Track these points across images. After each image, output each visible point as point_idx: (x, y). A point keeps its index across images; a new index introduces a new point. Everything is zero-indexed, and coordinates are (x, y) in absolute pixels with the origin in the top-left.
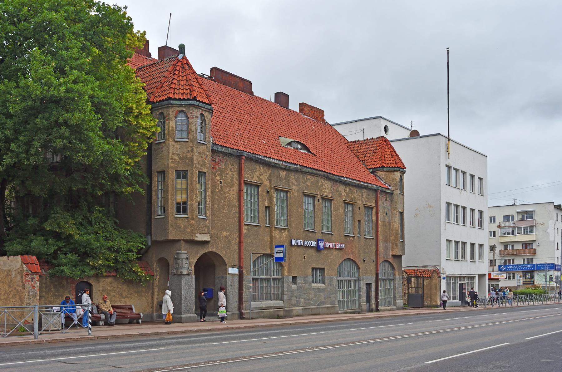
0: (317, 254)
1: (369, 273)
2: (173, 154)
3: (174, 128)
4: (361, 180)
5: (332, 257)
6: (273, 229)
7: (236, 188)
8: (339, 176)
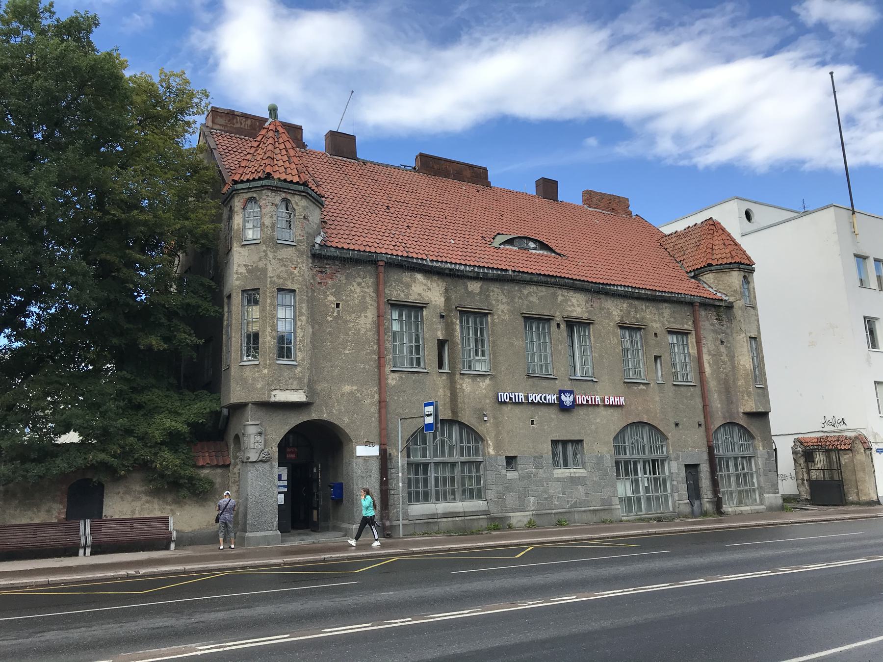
0: (563, 417)
1: (692, 447)
2: (239, 266)
3: (241, 226)
4: (654, 288)
5: (598, 420)
6: (458, 376)
7: (371, 314)
8: (603, 284)
